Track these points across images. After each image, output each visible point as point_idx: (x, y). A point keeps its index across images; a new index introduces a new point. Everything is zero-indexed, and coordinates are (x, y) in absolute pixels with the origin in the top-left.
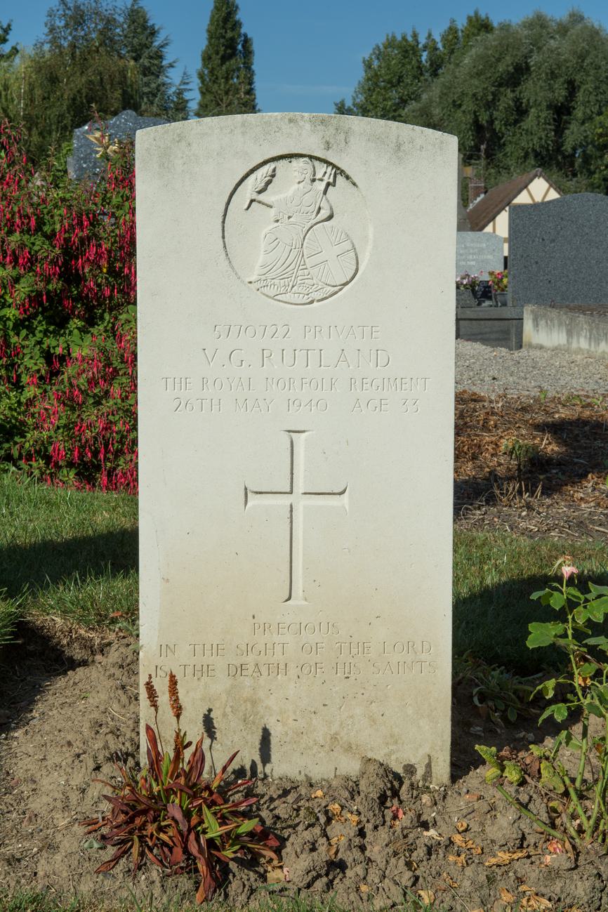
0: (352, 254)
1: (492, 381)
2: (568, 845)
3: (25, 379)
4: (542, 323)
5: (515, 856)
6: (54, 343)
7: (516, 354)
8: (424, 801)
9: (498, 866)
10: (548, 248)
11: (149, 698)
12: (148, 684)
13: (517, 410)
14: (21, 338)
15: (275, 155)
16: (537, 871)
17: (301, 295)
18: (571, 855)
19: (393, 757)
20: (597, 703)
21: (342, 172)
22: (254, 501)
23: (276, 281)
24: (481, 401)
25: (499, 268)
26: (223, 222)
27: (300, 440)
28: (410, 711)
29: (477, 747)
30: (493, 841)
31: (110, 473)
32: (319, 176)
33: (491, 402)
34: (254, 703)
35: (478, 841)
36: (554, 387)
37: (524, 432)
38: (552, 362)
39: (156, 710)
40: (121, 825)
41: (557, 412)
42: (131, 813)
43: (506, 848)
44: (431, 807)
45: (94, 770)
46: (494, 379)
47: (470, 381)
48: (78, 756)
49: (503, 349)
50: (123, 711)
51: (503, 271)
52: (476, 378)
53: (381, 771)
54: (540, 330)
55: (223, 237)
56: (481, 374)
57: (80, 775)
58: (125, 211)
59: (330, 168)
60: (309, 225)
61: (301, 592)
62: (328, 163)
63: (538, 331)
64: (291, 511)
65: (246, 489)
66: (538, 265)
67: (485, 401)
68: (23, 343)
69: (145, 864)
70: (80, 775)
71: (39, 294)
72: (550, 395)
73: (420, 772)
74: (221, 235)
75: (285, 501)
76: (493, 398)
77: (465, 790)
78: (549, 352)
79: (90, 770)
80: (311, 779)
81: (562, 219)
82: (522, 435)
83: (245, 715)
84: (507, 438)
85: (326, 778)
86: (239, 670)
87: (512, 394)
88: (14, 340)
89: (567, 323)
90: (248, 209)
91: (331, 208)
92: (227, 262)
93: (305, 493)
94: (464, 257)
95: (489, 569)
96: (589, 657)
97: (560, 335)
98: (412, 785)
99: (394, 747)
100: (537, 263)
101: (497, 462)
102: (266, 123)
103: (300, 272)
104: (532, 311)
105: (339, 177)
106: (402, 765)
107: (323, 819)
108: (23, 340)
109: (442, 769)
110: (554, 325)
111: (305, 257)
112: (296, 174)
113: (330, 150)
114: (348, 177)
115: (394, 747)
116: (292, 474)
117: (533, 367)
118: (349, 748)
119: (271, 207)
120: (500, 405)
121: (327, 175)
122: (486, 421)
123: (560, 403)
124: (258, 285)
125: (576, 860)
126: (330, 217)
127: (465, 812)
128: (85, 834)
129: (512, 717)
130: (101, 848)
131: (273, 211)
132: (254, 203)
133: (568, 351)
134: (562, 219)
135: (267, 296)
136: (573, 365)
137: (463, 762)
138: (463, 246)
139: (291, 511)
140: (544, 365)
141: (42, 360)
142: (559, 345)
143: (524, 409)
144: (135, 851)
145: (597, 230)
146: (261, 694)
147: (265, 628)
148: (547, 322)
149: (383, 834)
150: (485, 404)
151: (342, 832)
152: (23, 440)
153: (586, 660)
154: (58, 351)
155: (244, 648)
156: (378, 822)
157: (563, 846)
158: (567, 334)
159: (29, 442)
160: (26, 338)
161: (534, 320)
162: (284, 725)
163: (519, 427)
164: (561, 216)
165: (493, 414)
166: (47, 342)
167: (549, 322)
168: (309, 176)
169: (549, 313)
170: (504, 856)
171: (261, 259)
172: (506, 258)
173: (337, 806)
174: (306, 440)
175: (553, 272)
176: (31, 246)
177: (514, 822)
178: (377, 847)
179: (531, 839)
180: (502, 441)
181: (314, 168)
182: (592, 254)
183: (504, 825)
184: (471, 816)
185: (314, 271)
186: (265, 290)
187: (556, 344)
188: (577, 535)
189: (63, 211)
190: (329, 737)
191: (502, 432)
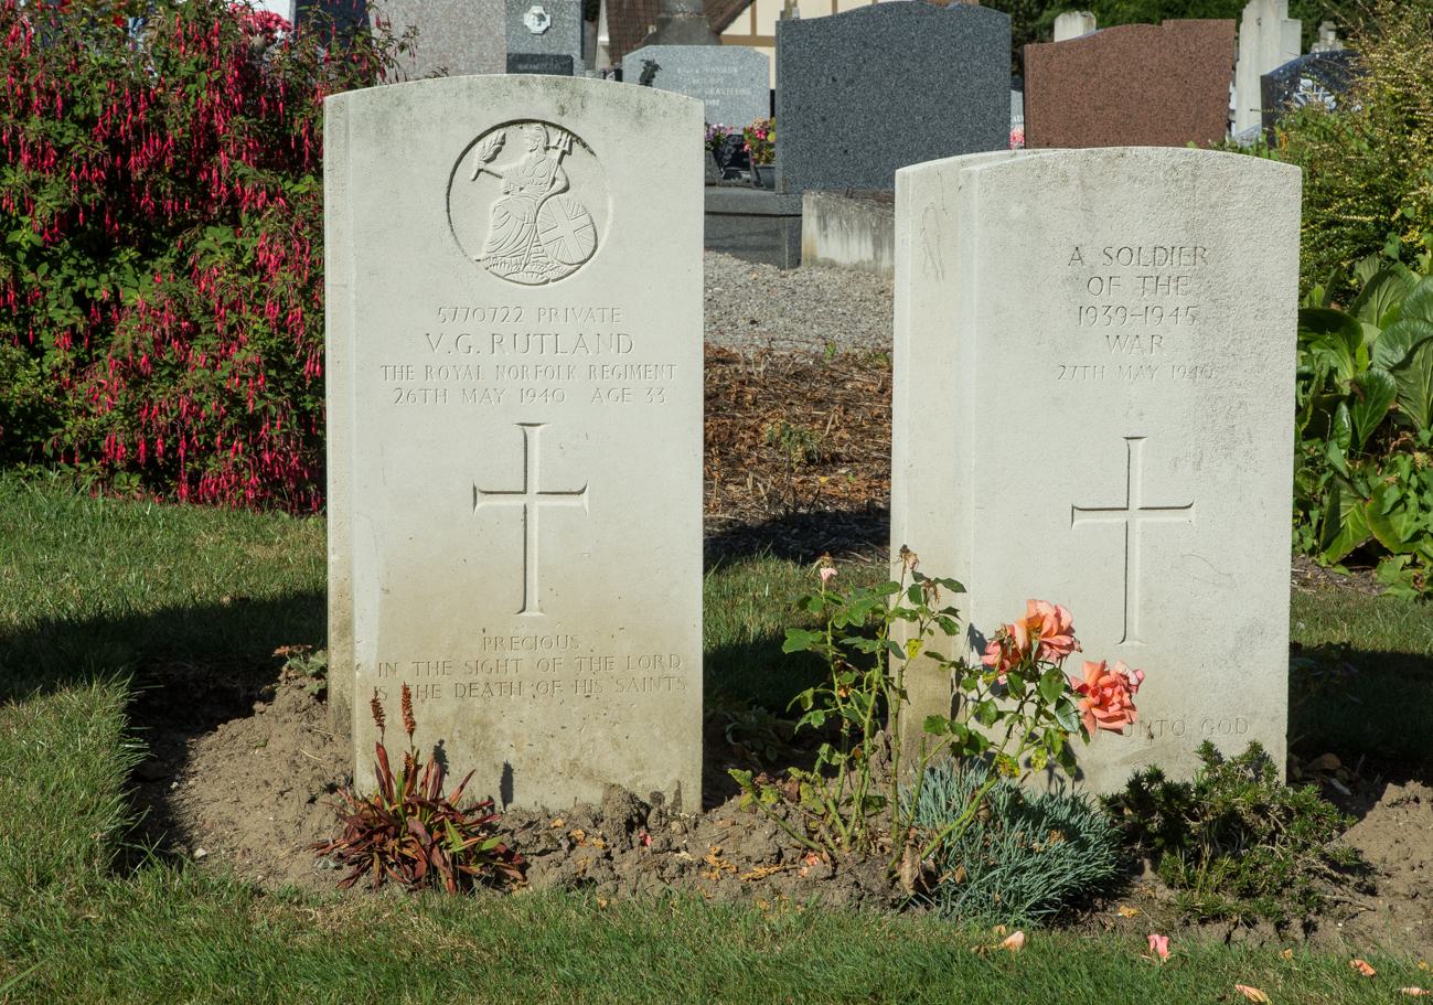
0: (591, 229)
1: (751, 326)
2: (825, 855)
3: (46, 338)
4: (833, 223)
5: (772, 870)
6: (91, 283)
7: (790, 277)
8: (673, 828)
9: (754, 880)
10: (842, 94)
11: (375, 717)
12: (374, 701)
13: (788, 376)
14: (40, 276)
15: (504, 121)
16: (794, 882)
17: (535, 275)
18: (829, 866)
19: (639, 784)
20: (856, 708)
21: (579, 139)
22: (483, 501)
23: (507, 259)
24: (732, 362)
25: (763, 114)
26: (448, 194)
27: (535, 435)
28: (657, 732)
29: (730, 771)
30: (748, 859)
31: (195, 478)
32: (553, 143)
33: (748, 363)
34: (485, 726)
35: (733, 861)
36: (849, 336)
37: (798, 411)
38: (848, 291)
39: (383, 731)
40: (359, 842)
41: (849, 380)
42: (368, 831)
43: (762, 864)
44: (682, 835)
45: (309, 802)
46: (753, 322)
47: (714, 327)
48: (282, 794)
49: (769, 266)
50: (318, 753)
51: (768, 119)
52: (724, 321)
53: (627, 798)
54: (830, 236)
55: (448, 211)
56: (731, 313)
57: (292, 809)
58: (200, 85)
59: (565, 135)
60: (543, 197)
61: (536, 601)
62: (563, 130)
63: (826, 236)
64: (525, 512)
65: (475, 489)
66: (826, 124)
67: (738, 362)
68: (45, 284)
69: (386, 881)
70: (292, 809)
71: (74, 210)
72: (841, 350)
73: (668, 801)
74: (445, 208)
75: (518, 501)
76: (751, 357)
77: (718, 818)
78: (844, 273)
79: (303, 803)
80: (548, 810)
81: (865, 44)
82: (795, 416)
83: (475, 740)
84: (772, 420)
85: (564, 808)
86: (468, 690)
87: (782, 349)
88: (29, 278)
89: (874, 225)
90: (474, 180)
91: (567, 179)
92: (453, 238)
93: (540, 493)
94: (699, 91)
95: (744, 603)
96: (850, 666)
97: (863, 242)
98: (660, 812)
99: (640, 773)
100: (824, 119)
101: (758, 457)
102: (494, 85)
103: (533, 249)
104: (817, 203)
105: (575, 144)
106: (649, 793)
107: (565, 845)
108: (44, 278)
109: (693, 797)
110: (852, 228)
111: (539, 232)
112: (528, 141)
113: (566, 116)
114: (584, 145)
115: (640, 773)
116: (526, 471)
117: (818, 301)
118: (590, 776)
119: (501, 177)
120: (761, 369)
121: (562, 143)
122: (740, 394)
123: (855, 365)
124: (487, 263)
125: (834, 871)
126: (566, 189)
127: (718, 839)
128: (317, 857)
129: (772, 757)
130: (337, 868)
131: (502, 183)
132: (481, 173)
133: (875, 271)
134: (865, 44)
135: (497, 275)
136: (882, 297)
137: (716, 791)
138: (697, 72)
139: (525, 512)
140: (835, 297)
141: (77, 310)
142: (861, 261)
143: (800, 375)
144: (376, 867)
145: (925, 64)
146: (492, 716)
147: (497, 642)
148: (841, 222)
149: (632, 855)
150: (739, 367)
151: (586, 857)
152: (60, 430)
153: (846, 668)
154: (102, 294)
155: (473, 665)
156: (625, 847)
157: (821, 858)
158: (874, 244)
159: (70, 433)
160: (48, 276)
161: (819, 217)
162: (518, 750)
163: (791, 404)
164: (863, 39)
165: (751, 383)
166: (80, 282)
167: (844, 222)
168: (542, 144)
169: (843, 207)
170: (761, 871)
171: (490, 234)
172: (772, 92)
173: (580, 832)
174: (541, 433)
175: (850, 134)
176: (58, 137)
177: (771, 837)
178: (626, 865)
179: (788, 855)
180: (765, 425)
181: (547, 133)
182: (916, 105)
183: (759, 842)
184: (724, 842)
185: (548, 248)
186: (495, 269)
187: (856, 260)
188: (869, 560)
189: (103, 85)
190: (568, 763)
191: (765, 412)
